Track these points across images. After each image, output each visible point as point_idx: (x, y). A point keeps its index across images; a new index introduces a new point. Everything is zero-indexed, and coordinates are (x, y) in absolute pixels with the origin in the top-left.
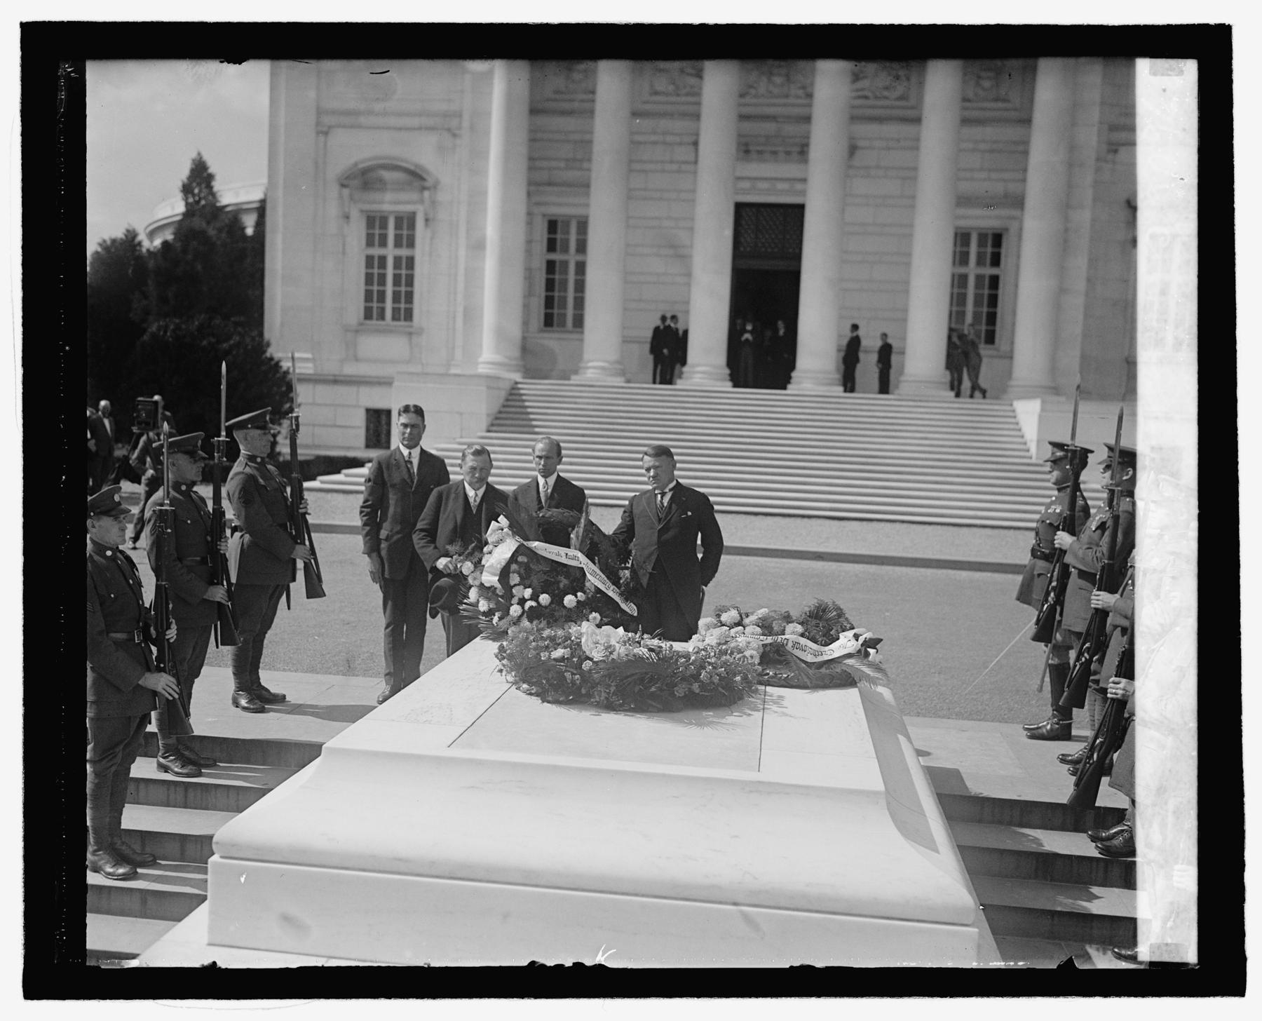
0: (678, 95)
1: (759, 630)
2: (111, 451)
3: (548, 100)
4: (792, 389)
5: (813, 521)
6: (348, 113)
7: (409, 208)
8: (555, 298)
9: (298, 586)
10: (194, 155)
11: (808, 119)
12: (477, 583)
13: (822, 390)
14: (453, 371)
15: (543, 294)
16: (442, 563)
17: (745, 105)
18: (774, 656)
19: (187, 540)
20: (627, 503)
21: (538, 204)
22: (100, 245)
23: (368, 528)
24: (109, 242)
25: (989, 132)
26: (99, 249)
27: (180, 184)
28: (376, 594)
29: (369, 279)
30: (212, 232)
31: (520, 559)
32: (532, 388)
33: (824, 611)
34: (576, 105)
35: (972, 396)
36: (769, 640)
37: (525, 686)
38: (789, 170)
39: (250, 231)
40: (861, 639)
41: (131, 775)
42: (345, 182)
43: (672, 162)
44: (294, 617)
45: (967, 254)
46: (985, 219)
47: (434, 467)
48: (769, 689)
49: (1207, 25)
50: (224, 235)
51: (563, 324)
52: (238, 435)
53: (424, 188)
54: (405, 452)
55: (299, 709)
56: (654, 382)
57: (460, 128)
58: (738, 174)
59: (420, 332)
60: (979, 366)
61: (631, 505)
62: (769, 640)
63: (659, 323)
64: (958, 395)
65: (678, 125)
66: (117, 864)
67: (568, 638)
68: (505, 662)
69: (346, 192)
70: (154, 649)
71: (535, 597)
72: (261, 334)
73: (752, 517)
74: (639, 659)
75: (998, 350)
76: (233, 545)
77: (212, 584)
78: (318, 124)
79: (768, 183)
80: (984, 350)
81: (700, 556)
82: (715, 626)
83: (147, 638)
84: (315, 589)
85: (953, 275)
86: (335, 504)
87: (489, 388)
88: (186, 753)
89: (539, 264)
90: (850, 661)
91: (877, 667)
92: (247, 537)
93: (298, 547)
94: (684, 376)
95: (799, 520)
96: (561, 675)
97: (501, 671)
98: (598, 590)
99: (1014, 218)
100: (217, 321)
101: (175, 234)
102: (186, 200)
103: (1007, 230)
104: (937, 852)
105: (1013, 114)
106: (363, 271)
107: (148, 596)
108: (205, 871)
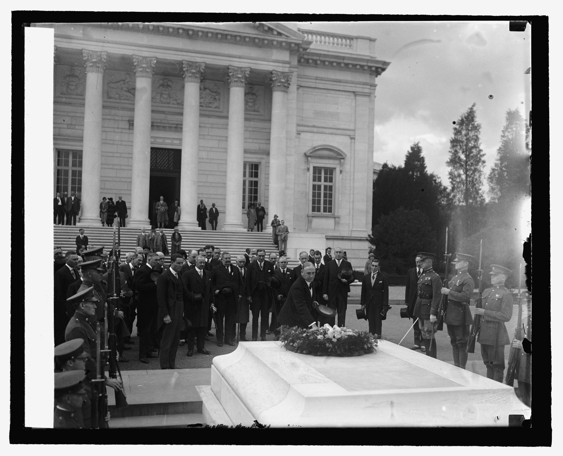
17: (247, 114)
34: (71, 101)
43: (118, 128)
46: (254, 159)
56: (258, 231)
75: (334, 215)
79: (167, 140)
99: (263, 158)
103: (260, 163)
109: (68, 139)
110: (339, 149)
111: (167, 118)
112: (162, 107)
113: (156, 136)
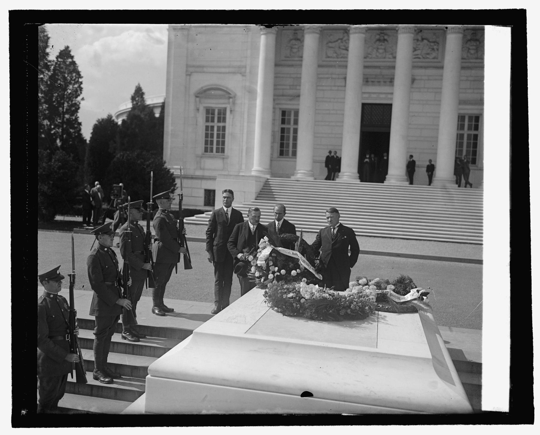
0: (338, 58)
1: (375, 287)
2: (101, 206)
3: (283, 60)
4: (386, 183)
5: (395, 240)
6: (198, 67)
7: (224, 106)
8: (284, 144)
9: (181, 264)
10: (137, 84)
11: (394, 67)
12: (255, 264)
13: (399, 183)
14: (241, 174)
15: (279, 142)
16: (240, 256)
17: (345, 61)
18: (382, 298)
19: (136, 243)
20: (318, 231)
21: (277, 104)
22: (97, 121)
23: (208, 240)
24: (101, 120)
26: (97, 123)
27: (130, 96)
28: (211, 267)
29: (207, 136)
30: (142, 116)
31: (273, 255)
32: (275, 182)
33: (404, 280)
34: (294, 63)
35: (466, 187)
36: (380, 291)
37: (276, 308)
38: (386, 89)
39: (157, 115)
40: (420, 292)
41: (112, 340)
42: (198, 95)
43: (335, 86)
44: (179, 276)
45: (464, 125)
46: (470, 110)
47: (237, 215)
48: (380, 313)
49: (516, 9)
50: (147, 117)
51: (288, 154)
52: (158, 202)
53: (230, 98)
54: (225, 209)
55: (179, 315)
57: (245, 73)
58: (363, 91)
59: (227, 158)
60: (469, 173)
61: (320, 232)
62: (380, 291)
63: (328, 154)
64: (459, 186)
65: (338, 70)
66: (105, 377)
67: (294, 289)
68: (267, 298)
69: (198, 99)
70: (122, 289)
71: (279, 271)
72: (162, 158)
73: (369, 238)
74: (325, 299)
75: (477, 167)
76: (154, 246)
77: (145, 262)
78: (187, 71)
79: (376, 95)
80: (471, 167)
81: (349, 254)
82: (356, 285)
83: (120, 284)
84: (188, 265)
85: (457, 134)
86: (196, 229)
87: (256, 181)
88: (134, 332)
89: (278, 129)
90: (415, 302)
91: (427, 305)
92: (161, 243)
93: (181, 248)
95: (389, 239)
96: (291, 304)
97: (265, 302)
98: (305, 269)
100: (144, 153)
101: (127, 117)
102: (132, 102)
104: (455, 385)
106: (204, 132)
107: (121, 266)
108: (144, 382)
111: (378, 74)
112: (377, 62)
113: (370, 91)
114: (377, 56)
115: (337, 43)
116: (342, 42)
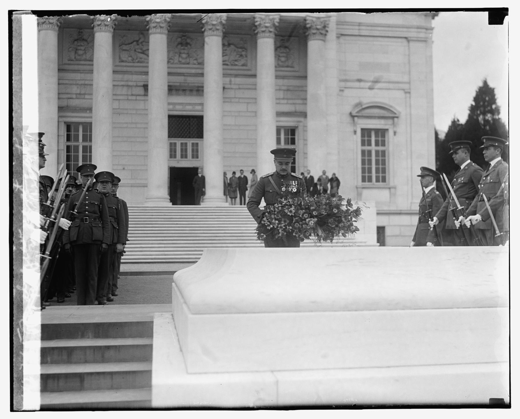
0: (134, 62)
25: (286, 82)
43: (132, 95)
46: (288, 122)
63: (321, 174)
79: (185, 105)
85: (91, 141)
94: (205, 201)
103: (297, 127)
105: (297, 74)
109: (76, 109)
110: (391, 107)
114: (179, 61)
115: (132, 45)
116: (138, 45)
